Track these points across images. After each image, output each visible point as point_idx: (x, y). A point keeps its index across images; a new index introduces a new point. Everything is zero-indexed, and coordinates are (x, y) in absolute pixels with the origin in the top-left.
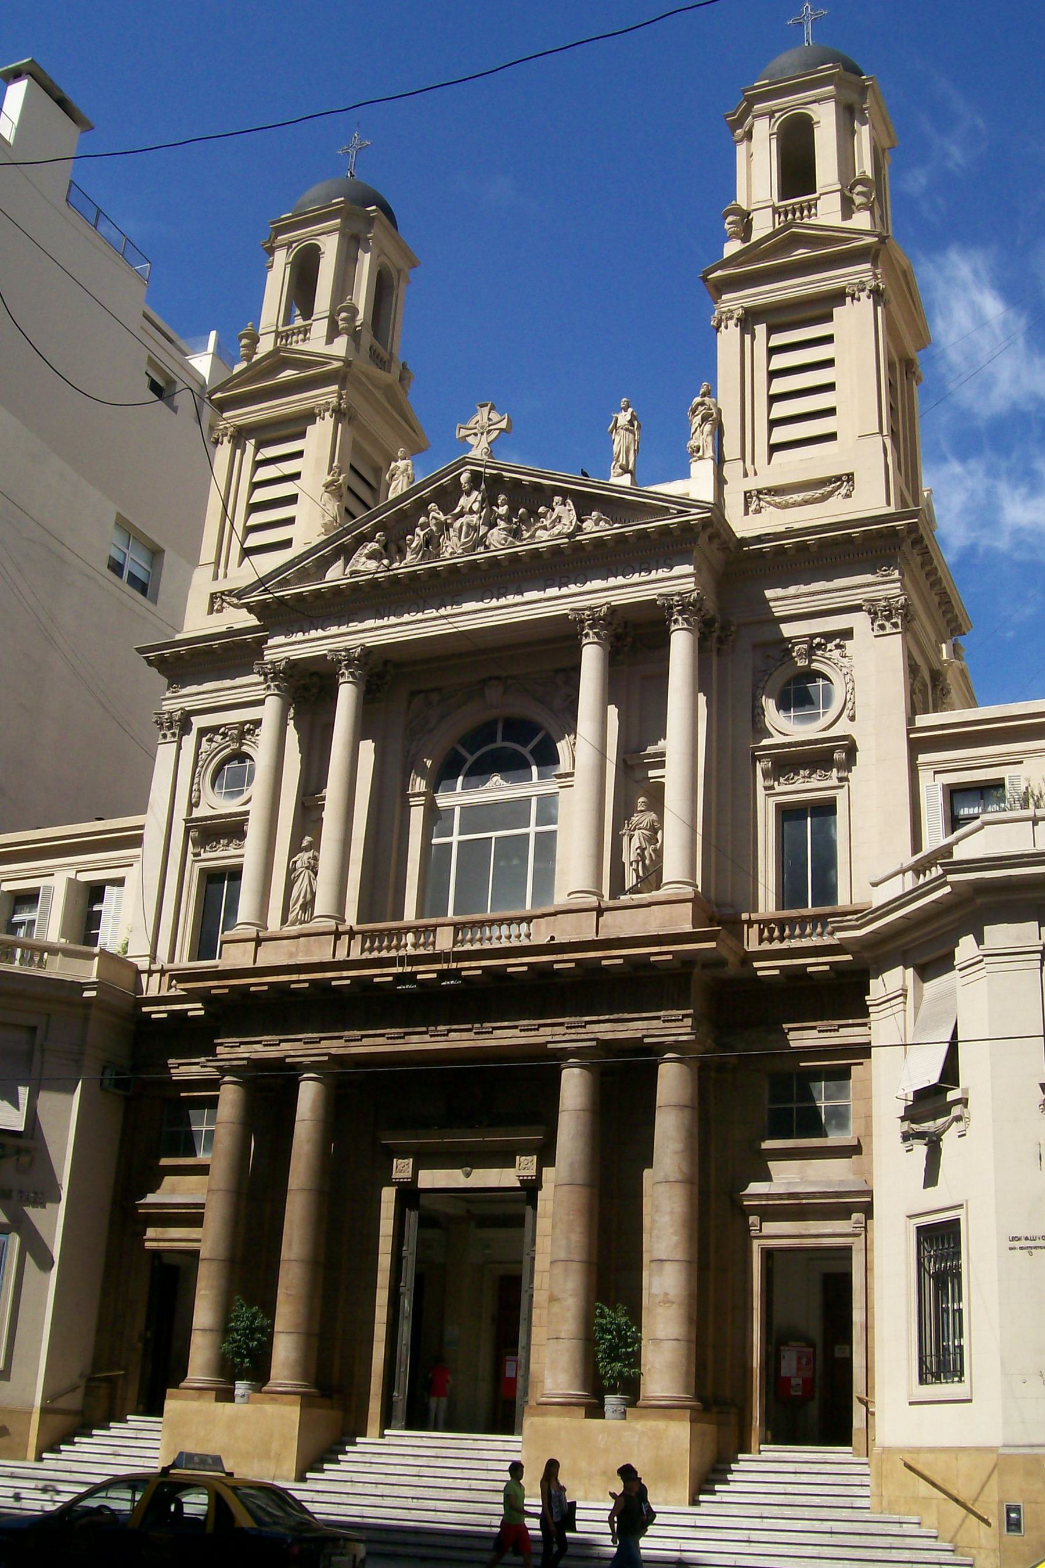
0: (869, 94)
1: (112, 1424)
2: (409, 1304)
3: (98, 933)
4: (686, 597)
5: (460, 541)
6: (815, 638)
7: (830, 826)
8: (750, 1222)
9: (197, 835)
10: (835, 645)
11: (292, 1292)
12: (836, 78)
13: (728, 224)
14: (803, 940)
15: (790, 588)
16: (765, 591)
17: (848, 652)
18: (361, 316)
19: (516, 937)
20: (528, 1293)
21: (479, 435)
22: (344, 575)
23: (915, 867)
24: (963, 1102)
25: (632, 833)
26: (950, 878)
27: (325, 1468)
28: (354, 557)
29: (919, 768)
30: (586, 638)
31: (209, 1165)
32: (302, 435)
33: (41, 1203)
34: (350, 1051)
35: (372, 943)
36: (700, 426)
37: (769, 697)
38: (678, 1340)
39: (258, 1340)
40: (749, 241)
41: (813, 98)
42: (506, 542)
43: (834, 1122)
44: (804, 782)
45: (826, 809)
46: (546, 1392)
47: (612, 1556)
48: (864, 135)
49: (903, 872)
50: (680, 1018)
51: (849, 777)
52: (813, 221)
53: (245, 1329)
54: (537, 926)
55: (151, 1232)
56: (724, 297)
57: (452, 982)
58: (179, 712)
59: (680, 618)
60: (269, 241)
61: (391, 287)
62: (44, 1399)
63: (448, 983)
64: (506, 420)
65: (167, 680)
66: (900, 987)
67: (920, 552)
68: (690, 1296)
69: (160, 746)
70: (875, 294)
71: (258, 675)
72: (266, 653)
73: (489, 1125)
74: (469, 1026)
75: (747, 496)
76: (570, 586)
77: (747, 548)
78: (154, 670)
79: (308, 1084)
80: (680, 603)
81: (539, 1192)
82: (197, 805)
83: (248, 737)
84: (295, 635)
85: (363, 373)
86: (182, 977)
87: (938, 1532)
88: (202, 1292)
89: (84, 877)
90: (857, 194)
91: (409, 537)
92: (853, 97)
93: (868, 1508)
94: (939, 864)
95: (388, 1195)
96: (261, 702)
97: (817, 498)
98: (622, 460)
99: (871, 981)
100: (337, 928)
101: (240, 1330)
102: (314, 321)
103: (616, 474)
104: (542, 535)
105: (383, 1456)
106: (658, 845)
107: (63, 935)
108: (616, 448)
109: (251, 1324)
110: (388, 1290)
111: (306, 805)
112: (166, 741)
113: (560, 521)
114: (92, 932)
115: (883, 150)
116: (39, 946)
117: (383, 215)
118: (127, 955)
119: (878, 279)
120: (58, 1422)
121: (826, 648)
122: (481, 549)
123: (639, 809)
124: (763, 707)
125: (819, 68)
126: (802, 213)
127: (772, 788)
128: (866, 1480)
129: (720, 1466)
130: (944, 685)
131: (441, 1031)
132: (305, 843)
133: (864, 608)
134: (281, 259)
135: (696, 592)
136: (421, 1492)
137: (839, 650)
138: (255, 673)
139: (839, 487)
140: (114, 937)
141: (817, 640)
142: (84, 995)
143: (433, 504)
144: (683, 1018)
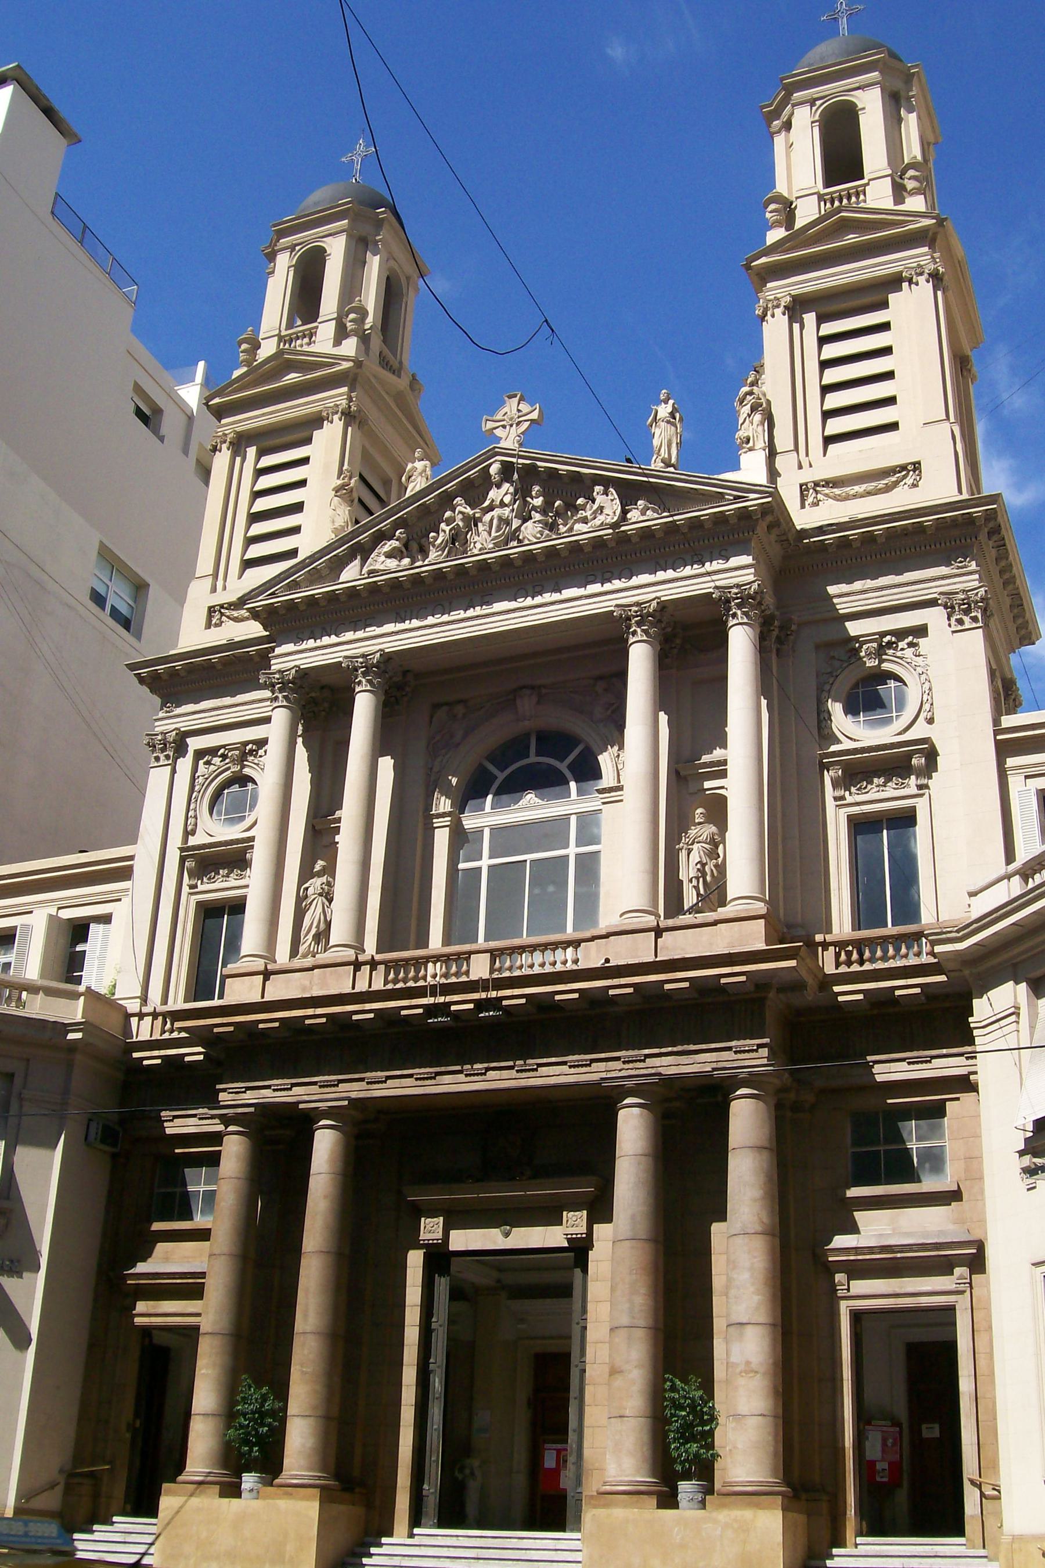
1: (95, 1527)
2: (440, 1382)
3: (81, 976)
4: (745, 589)
5: (490, 535)
7: (908, 839)
8: (836, 1281)
11: (309, 1370)
15: (855, 583)
16: (828, 588)
17: (922, 650)
19: (562, 963)
21: (508, 427)
22: (361, 575)
23: (1022, 871)
25: (690, 847)
28: (372, 556)
29: (1008, 773)
30: (633, 636)
31: (210, 1229)
32: (308, 441)
33: (17, 1272)
34: (372, 1094)
35: (397, 974)
36: (749, 416)
37: (835, 700)
38: (764, 1415)
39: (269, 1425)
41: (857, 85)
42: (542, 535)
43: (927, 1165)
44: (878, 791)
48: (911, 123)
49: (1008, 877)
50: (755, 1048)
51: (929, 784)
53: (253, 1413)
55: (141, 1306)
56: (769, 285)
57: (491, 1013)
58: (174, 732)
60: (270, 245)
61: (401, 295)
62: (19, 1496)
63: (487, 1014)
65: (160, 700)
66: (1012, 1005)
68: (775, 1364)
69: (152, 769)
70: (934, 278)
74: (511, 1063)
75: (803, 489)
76: (613, 581)
77: (808, 541)
78: (145, 689)
80: (739, 595)
82: (193, 833)
83: (251, 758)
84: (305, 642)
85: (375, 376)
88: (203, 1372)
89: (66, 914)
90: (909, 179)
91: (432, 534)
92: (898, 85)
95: (415, 1259)
96: (267, 720)
97: (880, 489)
98: (664, 453)
99: (975, 1001)
100: (357, 958)
101: (248, 1413)
102: (320, 323)
104: (580, 529)
105: (414, 1558)
106: (720, 860)
108: (656, 442)
110: (416, 1367)
111: (316, 828)
112: (159, 764)
113: (602, 512)
114: (75, 974)
115: (929, 144)
116: (17, 983)
118: (116, 997)
121: (897, 646)
122: (515, 543)
123: (697, 821)
124: (829, 711)
127: (843, 798)
130: (1016, 696)
131: (478, 1069)
133: (939, 602)
134: (284, 262)
135: (756, 583)
137: (912, 649)
139: (905, 477)
142: (68, 1038)
143: (459, 499)
144: (758, 1048)
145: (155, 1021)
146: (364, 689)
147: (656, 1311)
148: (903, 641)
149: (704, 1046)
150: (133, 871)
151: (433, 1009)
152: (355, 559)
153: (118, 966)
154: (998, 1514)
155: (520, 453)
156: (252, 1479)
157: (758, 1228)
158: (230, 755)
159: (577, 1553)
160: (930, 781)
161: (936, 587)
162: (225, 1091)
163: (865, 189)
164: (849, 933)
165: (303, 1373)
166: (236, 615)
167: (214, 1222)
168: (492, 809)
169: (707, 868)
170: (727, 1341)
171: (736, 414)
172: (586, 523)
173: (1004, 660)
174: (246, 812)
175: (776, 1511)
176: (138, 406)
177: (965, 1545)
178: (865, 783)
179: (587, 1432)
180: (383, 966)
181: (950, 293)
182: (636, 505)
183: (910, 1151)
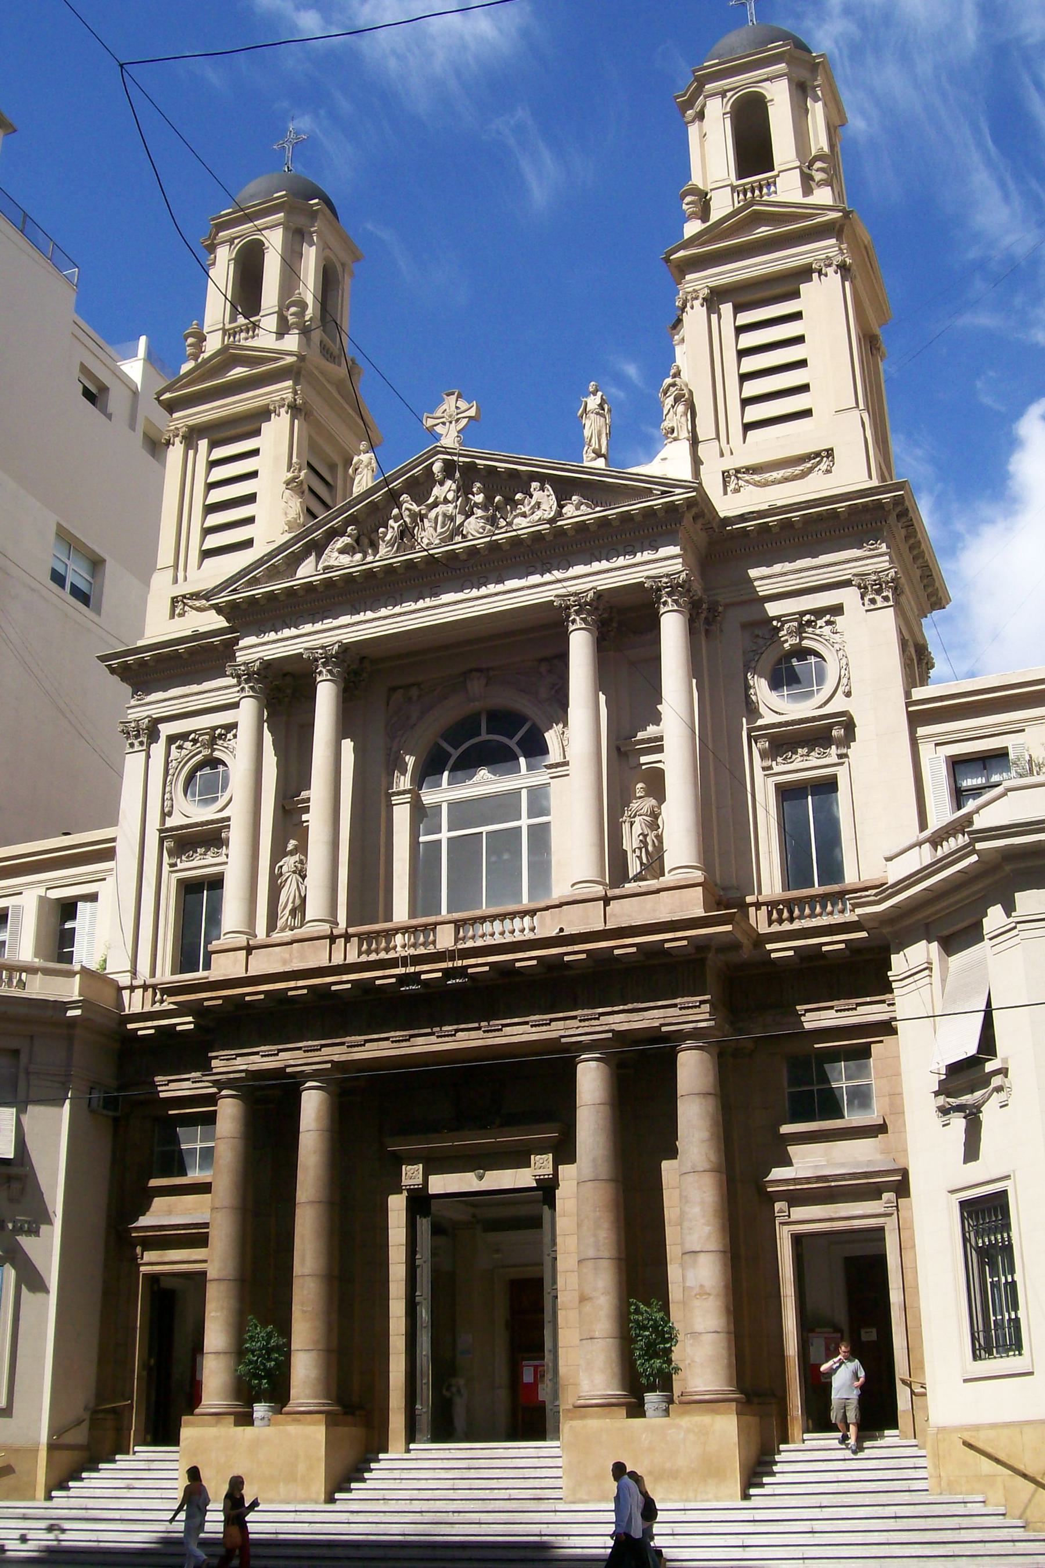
0: (820, 70)
1: (118, 1457)
2: (427, 1312)
3: (73, 951)
4: (675, 578)
5: (436, 531)
6: (805, 615)
7: (831, 804)
9: (172, 845)
10: (826, 622)
12: (787, 56)
13: (687, 204)
14: (813, 920)
17: (839, 627)
18: (309, 313)
19: (500, 934)
20: (551, 1295)
21: (448, 424)
22: (317, 571)
23: (931, 839)
24: (1003, 1072)
25: (633, 819)
26: (979, 846)
27: (352, 1487)
28: (326, 552)
29: (919, 741)
30: (573, 624)
31: (210, 1183)
32: (257, 433)
35: (369, 945)
36: (673, 407)
38: (718, 1332)
39: (276, 1360)
40: (708, 221)
41: (765, 76)
43: (856, 1102)
44: (803, 761)
45: (827, 786)
46: (581, 1394)
47: (607, 1557)
49: (920, 844)
50: (698, 1004)
52: (773, 198)
53: (261, 1349)
54: (542, 921)
56: (688, 277)
58: (147, 720)
59: (669, 600)
60: (209, 238)
61: (337, 282)
62: (50, 1435)
63: (454, 981)
64: (475, 407)
66: (926, 961)
67: (904, 526)
68: (726, 1287)
69: (127, 755)
70: (843, 269)
71: (231, 678)
72: (237, 654)
73: (501, 1126)
74: (476, 1025)
75: (726, 476)
76: (553, 572)
77: (730, 528)
78: (116, 678)
79: (310, 1093)
80: (669, 584)
81: (557, 1191)
82: (170, 814)
84: (267, 634)
85: (317, 368)
86: (171, 991)
87: (1006, 1509)
88: (212, 1315)
89: (54, 894)
90: (817, 171)
91: (381, 530)
92: (804, 74)
93: (927, 1490)
94: (967, 832)
95: (397, 1205)
96: (236, 705)
97: (797, 475)
101: (256, 1350)
103: (589, 459)
104: (519, 522)
105: (412, 1471)
107: (36, 955)
108: (587, 433)
109: (267, 1344)
110: (404, 1300)
111: (286, 808)
113: (539, 508)
114: (65, 950)
117: (327, 208)
118: (107, 971)
119: (843, 254)
120: (66, 1458)
121: (816, 624)
122: (458, 538)
125: (769, 46)
126: (761, 191)
127: (770, 768)
128: (920, 1462)
129: (768, 1458)
130: (928, 659)
131: (448, 1031)
132: (290, 847)
133: (854, 583)
135: (684, 573)
136: (462, 1506)
137: (829, 626)
138: (228, 676)
139: (819, 463)
140: (90, 954)
141: (218, 732)
142: (68, 1015)
143: (405, 496)
144: (700, 1004)
145: (145, 993)
146: (324, 678)
147: (619, 1242)
148: (821, 619)
149: (652, 1004)
150: (115, 851)
151: (404, 978)
152: (311, 555)
153: (107, 943)
154: (925, 1408)
155: (461, 452)
156: (262, 1409)
157: (706, 1165)
158: (200, 739)
159: (557, 1459)
160: (849, 750)
161: (850, 568)
162: (217, 1059)
163: (775, 181)
164: (780, 894)
165: (304, 1312)
166: (198, 605)
167: (214, 1176)
168: (448, 785)
169: (648, 839)
170: (683, 1267)
171: (660, 406)
172: (525, 517)
173: (916, 629)
174: (218, 793)
175: (731, 1416)
176: (85, 387)
177: (898, 1436)
178: (790, 753)
179: (561, 1352)
180: (356, 939)
181: (858, 281)
182: (571, 500)
183: (837, 1092)
